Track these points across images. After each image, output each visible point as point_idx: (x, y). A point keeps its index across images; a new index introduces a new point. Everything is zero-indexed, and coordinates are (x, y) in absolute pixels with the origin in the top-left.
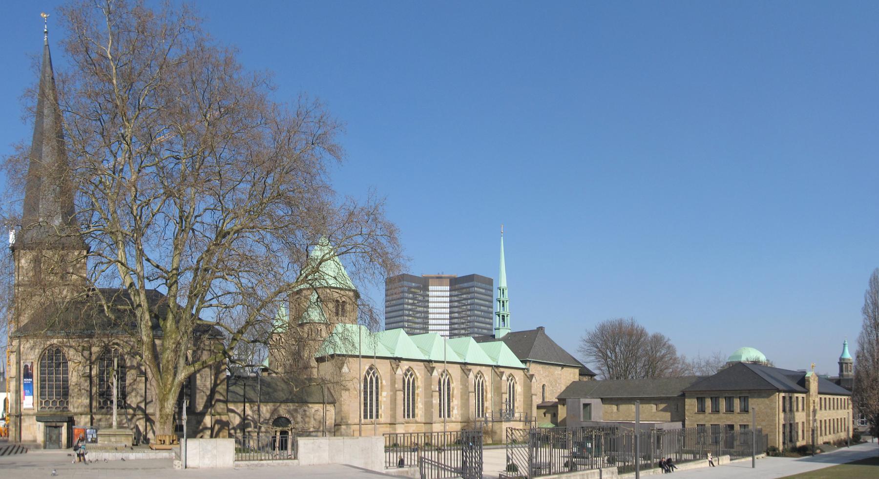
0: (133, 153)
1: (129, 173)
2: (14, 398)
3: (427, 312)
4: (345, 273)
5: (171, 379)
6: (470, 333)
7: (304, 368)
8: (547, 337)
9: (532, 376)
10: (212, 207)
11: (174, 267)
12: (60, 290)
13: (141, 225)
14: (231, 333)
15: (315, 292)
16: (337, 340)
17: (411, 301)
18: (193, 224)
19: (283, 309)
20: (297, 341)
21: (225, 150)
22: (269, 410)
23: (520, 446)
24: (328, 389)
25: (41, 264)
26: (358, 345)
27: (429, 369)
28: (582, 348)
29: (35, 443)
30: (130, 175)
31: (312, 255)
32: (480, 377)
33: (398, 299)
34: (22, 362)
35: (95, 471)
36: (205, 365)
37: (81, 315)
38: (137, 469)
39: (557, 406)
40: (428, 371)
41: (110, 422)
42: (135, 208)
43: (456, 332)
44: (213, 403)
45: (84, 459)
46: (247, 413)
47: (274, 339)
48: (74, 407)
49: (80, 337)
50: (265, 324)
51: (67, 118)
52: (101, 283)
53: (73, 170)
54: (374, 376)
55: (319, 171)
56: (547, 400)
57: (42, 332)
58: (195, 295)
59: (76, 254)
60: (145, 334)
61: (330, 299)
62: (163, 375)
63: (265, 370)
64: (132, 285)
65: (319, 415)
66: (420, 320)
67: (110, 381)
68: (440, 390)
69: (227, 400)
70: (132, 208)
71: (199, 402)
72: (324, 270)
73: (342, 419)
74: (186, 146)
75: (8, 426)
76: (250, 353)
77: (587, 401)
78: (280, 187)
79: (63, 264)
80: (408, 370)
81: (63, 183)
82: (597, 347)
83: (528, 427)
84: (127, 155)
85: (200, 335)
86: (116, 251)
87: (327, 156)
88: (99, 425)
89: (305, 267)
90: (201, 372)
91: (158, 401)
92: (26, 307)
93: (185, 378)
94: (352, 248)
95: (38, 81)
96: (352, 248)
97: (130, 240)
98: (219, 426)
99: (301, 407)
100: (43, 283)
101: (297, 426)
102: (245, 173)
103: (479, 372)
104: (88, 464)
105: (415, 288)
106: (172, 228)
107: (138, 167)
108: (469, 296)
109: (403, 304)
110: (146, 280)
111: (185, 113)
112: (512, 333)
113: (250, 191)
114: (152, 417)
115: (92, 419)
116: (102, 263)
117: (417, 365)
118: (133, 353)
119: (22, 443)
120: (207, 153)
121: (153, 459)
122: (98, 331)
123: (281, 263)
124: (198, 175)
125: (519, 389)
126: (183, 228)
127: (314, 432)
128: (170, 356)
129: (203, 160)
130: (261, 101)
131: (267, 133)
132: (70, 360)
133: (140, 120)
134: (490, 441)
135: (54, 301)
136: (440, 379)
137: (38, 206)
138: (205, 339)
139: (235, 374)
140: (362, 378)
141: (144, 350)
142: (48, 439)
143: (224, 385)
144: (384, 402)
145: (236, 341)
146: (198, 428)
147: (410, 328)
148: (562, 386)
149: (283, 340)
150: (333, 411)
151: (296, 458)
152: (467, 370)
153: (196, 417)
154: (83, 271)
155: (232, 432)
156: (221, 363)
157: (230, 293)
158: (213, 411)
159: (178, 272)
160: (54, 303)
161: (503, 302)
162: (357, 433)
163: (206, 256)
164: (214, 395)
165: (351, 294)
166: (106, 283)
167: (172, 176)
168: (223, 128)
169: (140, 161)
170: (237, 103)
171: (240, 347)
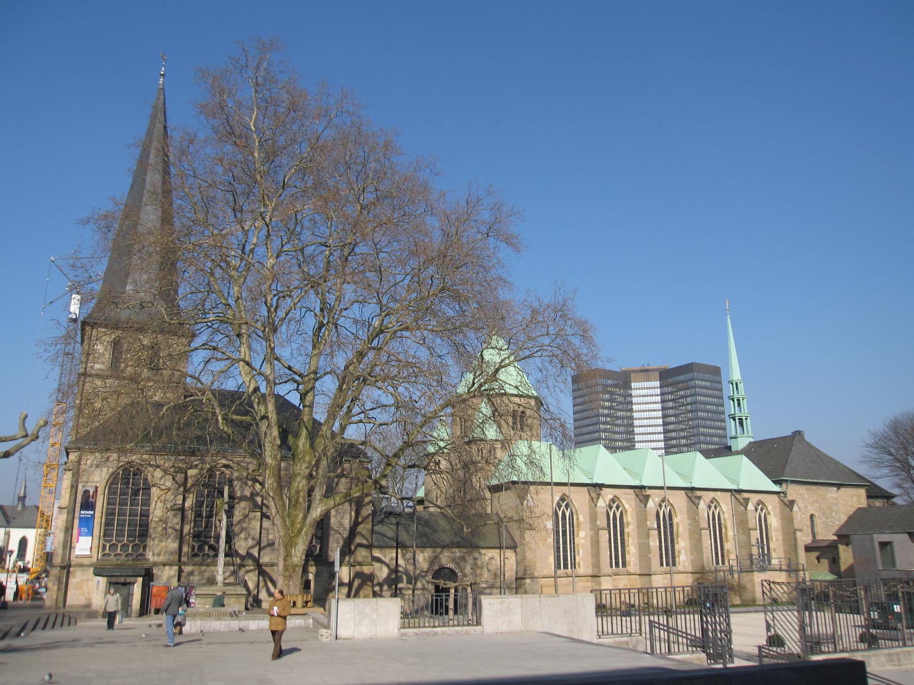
3: (631, 418)
5: (301, 515)
8: (808, 444)
17: (607, 404)
18: (338, 319)
22: (427, 558)
23: (785, 608)
27: (642, 498)
28: (865, 457)
32: (716, 507)
34: (80, 486)
39: (837, 547)
42: (269, 298)
48: (153, 554)
60: (270, 454)
63: (421, 502)
64: (257, 389)
66: (621, 429)
68: (659, 527)
73: (525, 570)
77: (885, 538)
80: (613, 501)
82: (890, 454)
83: (793, 580)
91: (282, 546)
98: (360, 581)
99: (470, 553)
105: (612, 386)
108: (688, 392)
112: (755, 443)
115: (180, 571)
117: (625, 494)
119: (67, 609)
125: (774, 522)
127: (489, 588)
131: (433, 223)
132: (154, 486)
134: (737, 601)
136: (658, 512)
141: (267, 476)
143: (368, 523)
144: (582, 545)
145: (390, 468)
147: (608, 440)
148: (842, 515)
150: (514, 559)
151: (478, 623)
155: (377, 589)
158: (352, 560)
161: (738, 400)
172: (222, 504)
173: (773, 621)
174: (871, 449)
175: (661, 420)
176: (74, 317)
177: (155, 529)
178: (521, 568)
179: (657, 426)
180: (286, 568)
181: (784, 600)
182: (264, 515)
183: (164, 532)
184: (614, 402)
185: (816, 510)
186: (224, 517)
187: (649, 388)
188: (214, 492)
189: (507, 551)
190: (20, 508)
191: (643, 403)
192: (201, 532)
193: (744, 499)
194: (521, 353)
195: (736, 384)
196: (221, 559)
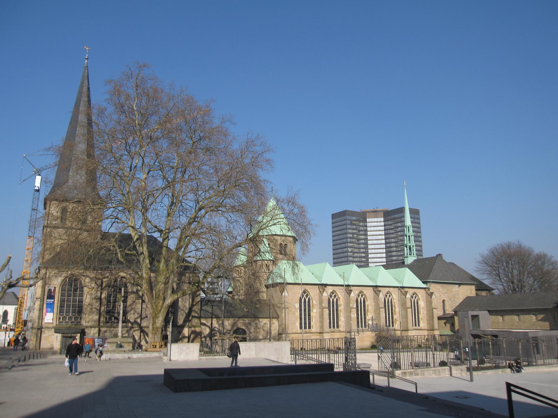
5: (161, 302)
22: (230, 324)
27: (348, 291)
29: (52, 350)
32: (390, 296)
39: (454, 318)
40: (347, 293)
46: (213, 326)
56: (447, 312)
71: (180, 318)
77: (475, 313)
80: (332, 293)
91: (151, 318)
98: (194, 335)
99: (254, 321)
103: (388, 292)
105: (355, 220)
109: (346, 233)
114: (146, 330)
115: (99, 331)
117: (339, 289)
119: (41, 350)
125: (422, 304)
132: (85, 286)
136: (357, 298)
142: (63, 347)
143: (199, 305)
144: (315, 316)
146: (179, 337)
150: (277, 324)
152: (378, 291)
153: (178, 329)
158: (190, 325)
161: (409, 236)
164: (192, 312)
172: (120, 297)
175: (384, 241)
176: (38, 189)
178: (281, 329)
179: (382, 244)
180: (153, 329)
182: (143, 301)
183: (91, 310)
185: (446, 297)
186: (122, 304)
188: (117, 289)
192: (110, 310)
196: (120, 324)
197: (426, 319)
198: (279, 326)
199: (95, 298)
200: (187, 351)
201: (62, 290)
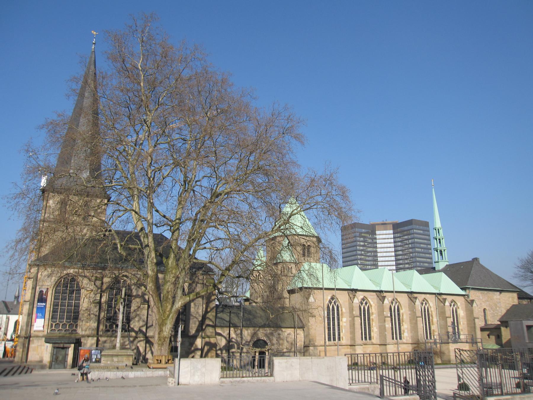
0: (152, 133)
1: (147, 147)
2: (26, 320)
3: (376, 252)
4: (310, 224)
5: (169, 307)
6: (414, 267)
7: (278, 299)
8: (482, 266)
9: (472, 301)
10: (209, 175)
11: (177, 218)
12: (81, 228)
13: (153, 185)
14: (220, 270)
15: (286, 238)
16: (305, 275)
17: (362, 243)
18: (194, 187)
19: (261, 252)
20: (272, 277)
21: (220, 137)
22: (250, 334)
23: (469, 365)
24: (298, 316)
25: (67, 205)
26: (321, 279)
27: (381, 298)
28: (516, 274)
29: (41, 364)
30: (148, 148)
31: (284, 210)
33: (352, 242)
34: (38, 288)
35: (97, 389)
36: (198, 296)
37: (97, 250)
38: (135, 386)
39: (500, 329)
40: (380, 299)
41: (114, 344)
42: (149, 172)
43: (401, 266)
44: (204, 328)
45: (87, 378)
46: (231, 336)
47: (255, 275)
48: (82, 330)
49: (94, 269)
50: (247, 263)
51: (102, 102)
52: (117, 226)
53: (103, 139)
54: (335, 305)
55: (288, 152)
57: (61, 263)
58: (193, 240)
59: (99, 201)
60: (150, 270)
61: (299, 244)
62: (163, 303)
63: (247, 300)
64: (142, 229)
65: (291, 338)
66: (370, 258)
67: (117, 308)
68: (391, 315)
69: (215, 325)
70: (147, 172)
72: (293, 221)
73: (310, 341)
74: (191, 132)
75: (16, 347)
76: (235, 286)
78: (260, 163)
79: (86, 208)
80: (363, 299)
81: (94, 147)
84: (147, 134)
85: (196, 271)
86: (132, 202)
87: (294, 141)
88: (104, 346)
89: (279, 220)
90: (195, 302)
91: (157, 325)
92: (48, 240)
93: (181, 306)
94: (314, 205)
95: (83, 73)
96: (314, 205)
97: (144, 195)
98: (208, 347)
99: (276, 331)
100: (66, 222)
101: (273, 347)
102: (234, 153)
104: (90, 383)
105: (365, 233)
106: (178, 188)
107: (154, 143)
108: (410, 237)
110: (154, 227)
111: (192, 110)
113: (238, 165)
115: (98, 341)
116: (119, 210)
117: (370, 295)
118: (139, 284)
119: (28, 363)
120: (206, 138)
121: (150, 377)
122: (110, 264)
123: (260, 217)
124: (200, 152)
125: (461, 313)
126: (186, 189)
127: (287, 352)
128: (170, 288)
129: (204, 143)
130: (246, 106)
132: (83, 288)
133: (159, 111)
134: (439, 361)
135: (74, 238)
137: (70, 161)
138: (199, 274)
139: (223, 303)
140: (326, 306)
142: (54, 360)
143: (213, 312)
144: (345, 326)
145: (224, 277)
146: (191, 349)
147: (363, 265)
149: (261, 276)
150: (303, 335)
151: (272, 375)
154: (102, 215)
155: (219, 352)
156: (211, 294)
157: (220, 239)
158: (203, 335)
159: (180, 221)
160: (75, 239)
161: (439, 239)
162: (323, 354)
163: (203, 210)
165: (315, 239)
166: (121, 226)
167: (180, 151)
168: (219, 122)
169: (156, 139)
170: (229, 106)
171: (227, 281)
173: (462, 375)
174: (520, 269)
175: (394, 253)
177: (83, 314)
179: (391, 256)
180: (159, 338)
181: (469, 360)
183: (89, 316)
184: (366, 242)
187: (387, 234)
189: (298, 329)
190: (15, 303)
191: (383, 243)
192: (111, 317)
193: (443, 299)
194: (304, 207)
195: (438, 230)
197: (467, 330)
198: (305, 337)
199: (94, 302)
200: (204, 370)
201: (56, 292)
